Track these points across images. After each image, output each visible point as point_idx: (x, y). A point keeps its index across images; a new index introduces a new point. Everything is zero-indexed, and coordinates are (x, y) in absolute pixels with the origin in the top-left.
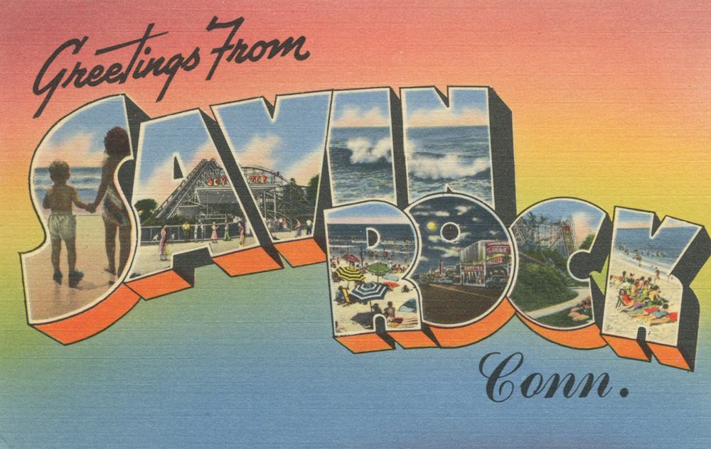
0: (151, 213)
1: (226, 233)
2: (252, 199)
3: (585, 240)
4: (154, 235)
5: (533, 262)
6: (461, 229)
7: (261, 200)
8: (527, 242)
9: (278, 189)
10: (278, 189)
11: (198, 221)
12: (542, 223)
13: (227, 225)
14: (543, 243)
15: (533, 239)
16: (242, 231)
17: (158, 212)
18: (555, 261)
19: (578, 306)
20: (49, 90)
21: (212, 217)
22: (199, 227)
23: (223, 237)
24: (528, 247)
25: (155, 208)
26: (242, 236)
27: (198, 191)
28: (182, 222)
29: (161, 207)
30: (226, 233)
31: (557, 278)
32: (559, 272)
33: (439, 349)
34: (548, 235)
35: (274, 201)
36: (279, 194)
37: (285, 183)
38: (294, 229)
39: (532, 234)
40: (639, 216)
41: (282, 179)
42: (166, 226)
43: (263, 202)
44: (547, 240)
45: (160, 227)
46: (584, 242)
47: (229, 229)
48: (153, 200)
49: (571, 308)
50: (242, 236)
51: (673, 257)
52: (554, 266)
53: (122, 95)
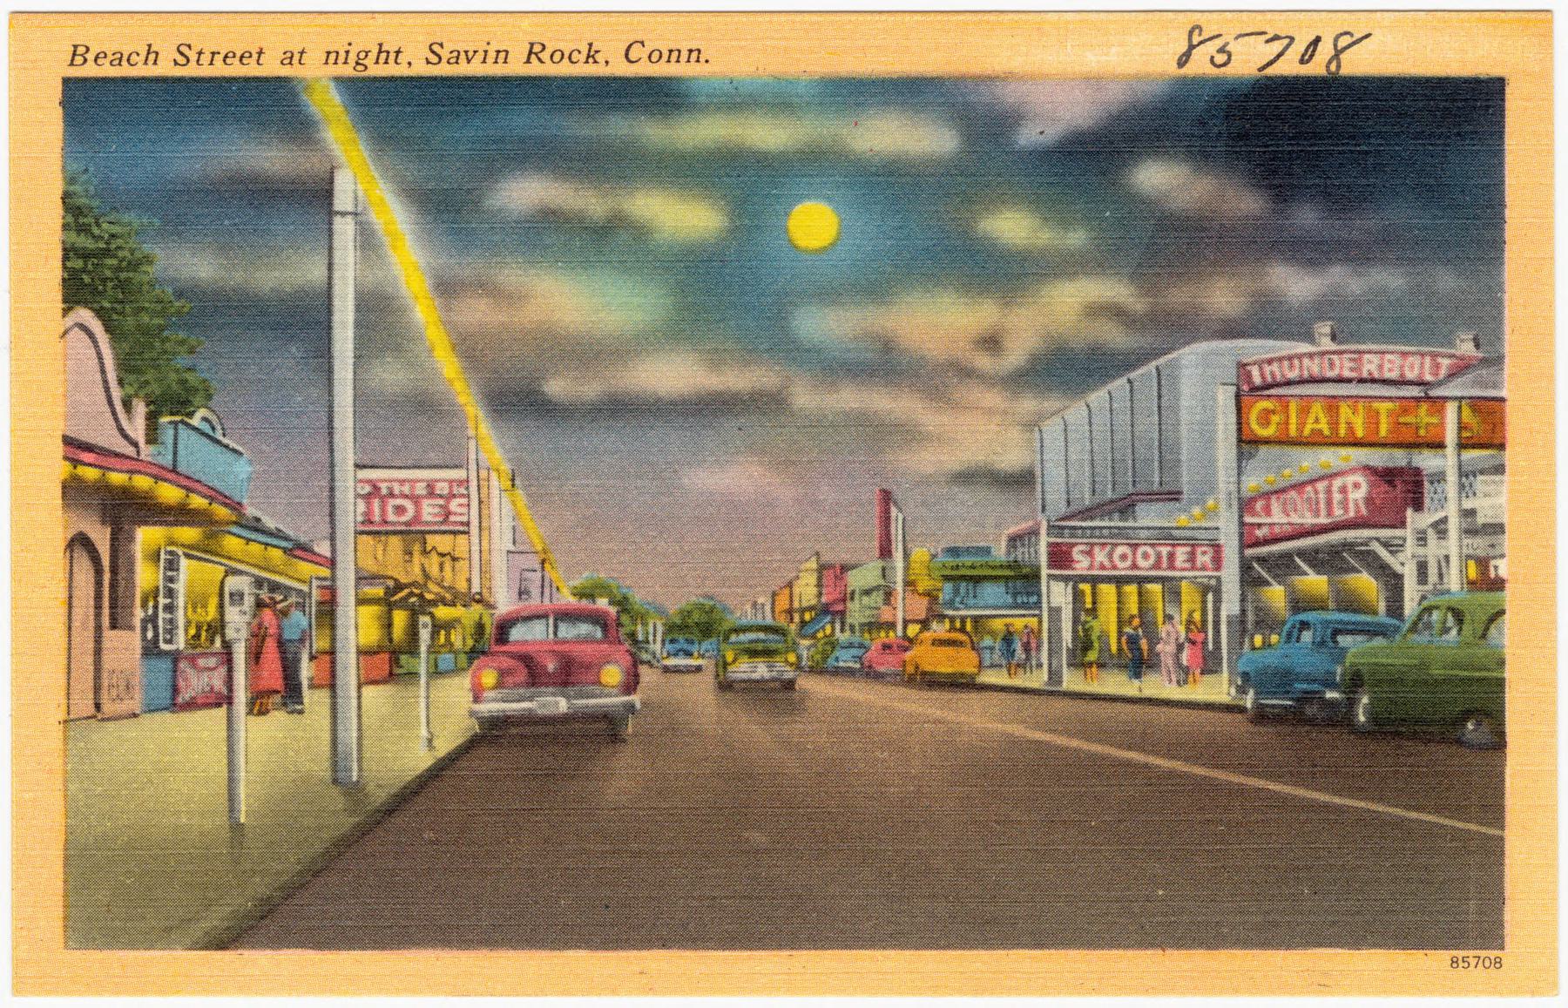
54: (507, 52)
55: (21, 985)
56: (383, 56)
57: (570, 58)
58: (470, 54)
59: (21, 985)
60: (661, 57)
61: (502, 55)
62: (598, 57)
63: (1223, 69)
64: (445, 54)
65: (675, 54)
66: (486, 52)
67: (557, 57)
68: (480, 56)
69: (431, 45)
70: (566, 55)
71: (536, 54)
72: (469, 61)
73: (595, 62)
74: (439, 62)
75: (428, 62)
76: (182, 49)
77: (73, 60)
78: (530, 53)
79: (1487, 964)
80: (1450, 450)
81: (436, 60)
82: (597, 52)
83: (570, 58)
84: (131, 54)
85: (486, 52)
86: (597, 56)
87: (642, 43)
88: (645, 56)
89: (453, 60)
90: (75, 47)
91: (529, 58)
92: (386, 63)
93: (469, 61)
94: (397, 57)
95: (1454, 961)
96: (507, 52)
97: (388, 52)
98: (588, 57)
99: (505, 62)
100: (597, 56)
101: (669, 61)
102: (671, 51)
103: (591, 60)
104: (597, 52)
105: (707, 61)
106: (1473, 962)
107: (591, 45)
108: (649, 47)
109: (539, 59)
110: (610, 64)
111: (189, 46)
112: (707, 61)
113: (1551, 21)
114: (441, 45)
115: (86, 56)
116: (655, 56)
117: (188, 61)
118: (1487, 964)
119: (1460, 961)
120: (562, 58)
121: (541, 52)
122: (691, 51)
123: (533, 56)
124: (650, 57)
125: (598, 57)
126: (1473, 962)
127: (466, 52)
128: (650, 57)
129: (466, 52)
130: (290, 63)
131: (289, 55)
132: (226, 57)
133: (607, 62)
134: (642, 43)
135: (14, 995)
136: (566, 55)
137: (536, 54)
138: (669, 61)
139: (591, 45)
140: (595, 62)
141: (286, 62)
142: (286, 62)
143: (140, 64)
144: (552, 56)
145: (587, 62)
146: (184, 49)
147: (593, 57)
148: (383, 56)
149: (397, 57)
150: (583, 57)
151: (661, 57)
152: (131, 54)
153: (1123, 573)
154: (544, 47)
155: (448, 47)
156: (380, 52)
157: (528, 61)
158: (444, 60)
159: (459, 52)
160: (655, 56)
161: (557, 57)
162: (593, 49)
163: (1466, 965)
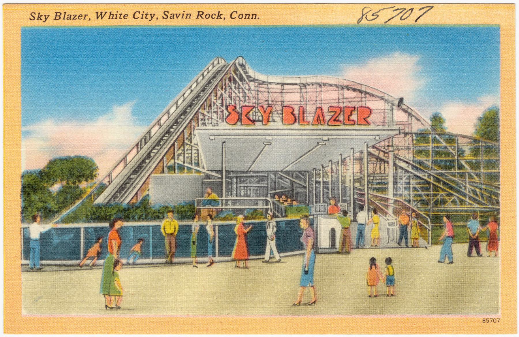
0: (82, 192)
1: (271, 245)
4: (89, 244)
6: (266, 197)
7: (357, 168)
9: (399, 141)
10: (399, 141)
11: (199, 212)
13: (273, 223)
16: (310, 240)
17: (102, 188)
20: (404, 238)
21: (234, 202)
22: (203, 228)
23: (263, 252)
26: (308, 251)
27: (201, 135)
28: (159, 215)
29: (109, 175)
30: (271, 245)
33: (408, 248)
35: (390, 170)
36: (402, 154)
37: (416, 127)
38: (435, 242)
40: (241, 201)
41: (410, 114)
42: (118, 225)
43: (361, 171)
45: (107, 225)
47: (277, 233)
50: (308, 251)
51: (256, 193)
53: (248, 118)
56: (112, 16)
58: (178, 15)
61: (189, 16)
62: (221, 16)
63: (372, 22)
64: (169, 15)
66: (183, 14)
67: (207, 16)
68: (181, 16)
69: (165, 12)
70: (211, 17)
72: (177, 18)
74: (167, 18)
75: (163, 18)
77: (55, 18)
78: (198, 15)
79: (495, 321)
80: (226, 198)
81: (166, 17)
82: (221, 15)
86: (221, 16)
88: (237, 17)
90: (57, 13)
91: (198, 16)
93: (177, 18)
94: (146, 16)
96: (256, 15)
97: (113, 15)
98: (38, 17)
100: (221, 16)
104: (221, 15)
106: (490, 320)
107: (219, 12)
108: (239, 13)
109: (201, 17)
114: (168, 12)
115: (61, 16)
116: (241, 17)
119: (486, 320)
121: (202, 14)
125: (221, 16)
127: (176, 14)
129: (176, 14)
130: (173, 18)
132: (124, 16)
133: (224, 18)
134: (236, 12)
136: (211, 17)
137: (200, 15)
139: (219, 12)
141: (172, 17)
142: (172, 17)
143: (83, 19)
145: (217, 18)
146: (166, 13)
147: (220, 16)
148: (112, 16)
149: (146, 16)
150: (216, 17)
153: (457, 195)
154: (203, 13)
155: (170, 13)
156: (110, 15)
158: (169, 17)
159: (174, 14)
161: (207, 16)
162: (220, 13)
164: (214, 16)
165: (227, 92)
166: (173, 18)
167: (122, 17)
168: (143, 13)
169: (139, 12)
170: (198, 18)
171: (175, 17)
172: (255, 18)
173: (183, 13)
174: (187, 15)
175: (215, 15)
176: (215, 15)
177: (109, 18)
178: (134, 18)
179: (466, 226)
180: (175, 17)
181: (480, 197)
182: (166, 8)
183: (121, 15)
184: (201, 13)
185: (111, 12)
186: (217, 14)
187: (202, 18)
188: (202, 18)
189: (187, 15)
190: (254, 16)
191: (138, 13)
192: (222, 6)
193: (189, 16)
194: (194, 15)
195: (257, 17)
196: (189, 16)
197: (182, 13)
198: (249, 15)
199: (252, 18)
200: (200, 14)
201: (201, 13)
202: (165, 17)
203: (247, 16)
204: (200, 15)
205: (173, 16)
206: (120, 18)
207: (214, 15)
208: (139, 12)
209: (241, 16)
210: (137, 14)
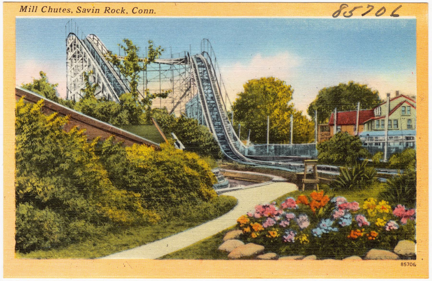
2: (152, 19)
3: (242, 90)
5: (141, 143)
8: (122, 102)
12: (151, 60)
14: (156, 103)
15: (135, 94)
18: (184, 138)
19: (239, 226)
24: (126, 111)
25: (212, 169)
31: (190, 171)
32: (194, 161)
34: (166, 86)
39: (134, 84)
44: (163, 96)
46: (243, 95)
48: (273, 82)
49: (225, 232)
52: (182, 147)
54: (153, 10)
55: (5, 276)
56: (51, 10)
57: (117, 12)
59: (5, 276)
60: (142, 11)
61: (98, 11)
64: (82, 10)
65: (56, 11)
66: (93, 9)
67: (113, 11)
68: (92, 10)
71: (107, 10)
73: (124, 13)
75: (77, 12)
76: (79, 8)
82: (124, 10)
83: (117, 12)
84: (117, 10)
85: (93, 9)
87: (137, 8)
88: (138, 12)
89: (84, 12)
90: (106, 8)
91: (105, 11)
92: (51, 12)
93: (88, 12)
95: (402, 264)
96: (99, 9)
97: (52, 9)
98: (122, 11)
99: (98, 12)
100: (124, 11)
101: (144, 13)
102: (145, 10)
103: (123, 12)
104: (124, 10)
105: (155, 13)
106: (407, 264)
110: (388, 92)
111: (81, 7)
112: (155, 13)
113: (428, 6)
116: (141, 11)
117: (80, 11)
118: (411, 265)
120: (114, 12)
122: (150, 10)
123: (106, 11)
124: (139, 11)
126: (407, 264)
127: (88, 9)
128: (139, 11)
129: (88, 9)
131: (84, 10)
132: (63, 10)
133: (127, 13)
134: (137, 8)
135: (4, 278)
138: (144, 13)
140: (124, 13)
144: (112, 11)
145: (121, 13)
148: (51, 10)
150: (120, 11)
151: (142, 11)
152: (117, 10)
156: (50, 9)
157: (105, 12)
160: (141, 11)
161: (113, 11)
163: (405, 265)
164: (118, 11)
165: (97, 74)
166: (85, 12)
167: (61, 11)
168: (30, 7)
169: (46, 7)
170: (105, 12)
171: (87, 11)
172: (152, 13)
173: (93, 8)
174: (96, 10)
175: (119, 10)
176: (119, 10)
177: (49, 12)
178: (42, 11)
179: (229, 179)
180: (87, 11)
181: (314, 131)
182: (80, 5)
183: (60, 9)
184: (108, 9)
185: (50, 7)
186: (121, 10)
187: (109, 12)
188: (109, 12)
189: (96, 10)
190: (152, 11)
191: (136, 9)
192: (154, 4)
193: (98, 11)
194: (102, 10)
195: (154, 12)
196: (98, 11)
197: (92, 8)
198: (147, 10)
199: (96, 12)
200: (107, 9)
201: (108, 9)
202: (79, 11)
203: (146, 11)
204: (107, 10)
205: (85, 11)
206: (60, 12)
207: (118, 10)
208: (46, 7)
209: (141, 11)
210: (135, 9)
